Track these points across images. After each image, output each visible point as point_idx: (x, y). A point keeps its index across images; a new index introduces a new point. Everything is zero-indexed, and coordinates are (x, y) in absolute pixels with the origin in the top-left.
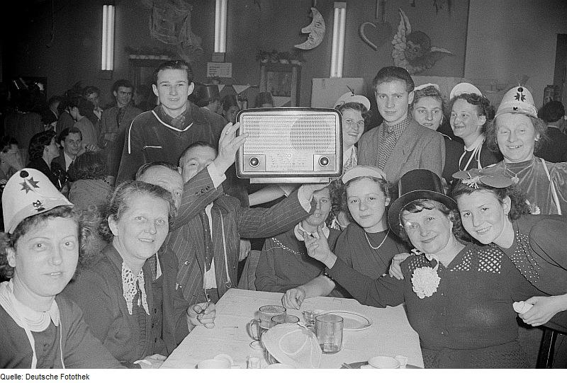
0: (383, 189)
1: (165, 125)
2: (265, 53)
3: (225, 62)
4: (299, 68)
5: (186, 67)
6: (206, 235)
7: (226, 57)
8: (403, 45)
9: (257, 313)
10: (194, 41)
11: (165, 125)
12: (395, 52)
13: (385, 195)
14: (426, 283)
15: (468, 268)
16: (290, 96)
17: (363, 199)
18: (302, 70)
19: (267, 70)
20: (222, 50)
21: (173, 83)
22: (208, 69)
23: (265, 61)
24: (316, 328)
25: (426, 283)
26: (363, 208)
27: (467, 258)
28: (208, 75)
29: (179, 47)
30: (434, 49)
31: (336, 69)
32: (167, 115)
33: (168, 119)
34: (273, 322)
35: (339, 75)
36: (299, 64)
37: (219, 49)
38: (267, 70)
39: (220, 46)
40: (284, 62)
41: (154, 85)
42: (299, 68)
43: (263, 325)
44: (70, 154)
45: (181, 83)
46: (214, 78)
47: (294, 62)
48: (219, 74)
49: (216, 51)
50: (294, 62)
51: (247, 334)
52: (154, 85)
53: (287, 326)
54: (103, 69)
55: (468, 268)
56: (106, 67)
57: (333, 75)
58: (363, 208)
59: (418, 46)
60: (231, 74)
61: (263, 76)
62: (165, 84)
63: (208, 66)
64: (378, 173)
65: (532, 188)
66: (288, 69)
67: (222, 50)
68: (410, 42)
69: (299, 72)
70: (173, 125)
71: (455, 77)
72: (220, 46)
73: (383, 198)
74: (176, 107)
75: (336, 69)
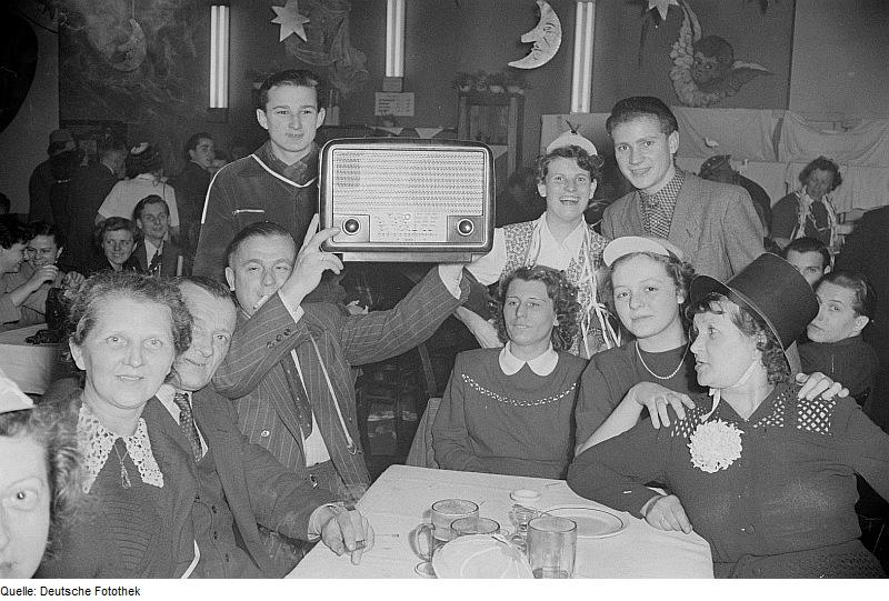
0: (672, 274)
1: (274, 174)
2: (466, 76)
3: (403, 92)
4: (521, 99)
5: (315, 83)
6: (291, 380)
7: (406, 83)
8: (689, 59)
9: (427, 514)
10: (352, 58)
11: (274, 174)
12: (675, 70)
13: (677, 284)
14: (715, 447)
15: (781, 423)
16: (507, 144)
17: (635, 291)
18: (527, 102)
19: (469, 104)
20: (398, 74)
21: (294, 108)
22: (377, 102)
23: (467, 89)
24: (529, 540)
25: (715, 447)
26: (635, 305)
27: (779, 406)
28: (377, 113)
29: (331, 69)
30: (738, 65)
31: (580, 100)
32: (279, 161)
33: (278, 166)
34: (456, 532)
35: (585, 109)
36: (521, 92)
37: (393, 72)
38: (469, 104)
39: (394, 66)
40: (496, 89)
41: (259, 112)
42: (521, 99)
43: (439, 535)
44: (153, 238)
45: (308, 109)
46: (386, 118)
47: (513, 90)
48: (393, 110)
49: (388, 74)
50: (513, 90)
51: (408, 547)
52: (259, 112)
53: (477, 539)
54: (212, 106)
55: (781, 423)
56: (217, 102)
57: (575, 109)
58: (635, 305)
59: (713, 60)
60: (412, 107)
61: (463, 115)
62: (280, 110)
63: (377, 99)
64: (659, 247)
65: (606, 330)
66: (504, 100)
67: (398, 74)
68: (700, 55)
69: (521, 107)
70: (289, 175)
71: (773, 109)
72: (394, 66)
73: (673, 288)
74: (296, 147)
75: (580, 100)
